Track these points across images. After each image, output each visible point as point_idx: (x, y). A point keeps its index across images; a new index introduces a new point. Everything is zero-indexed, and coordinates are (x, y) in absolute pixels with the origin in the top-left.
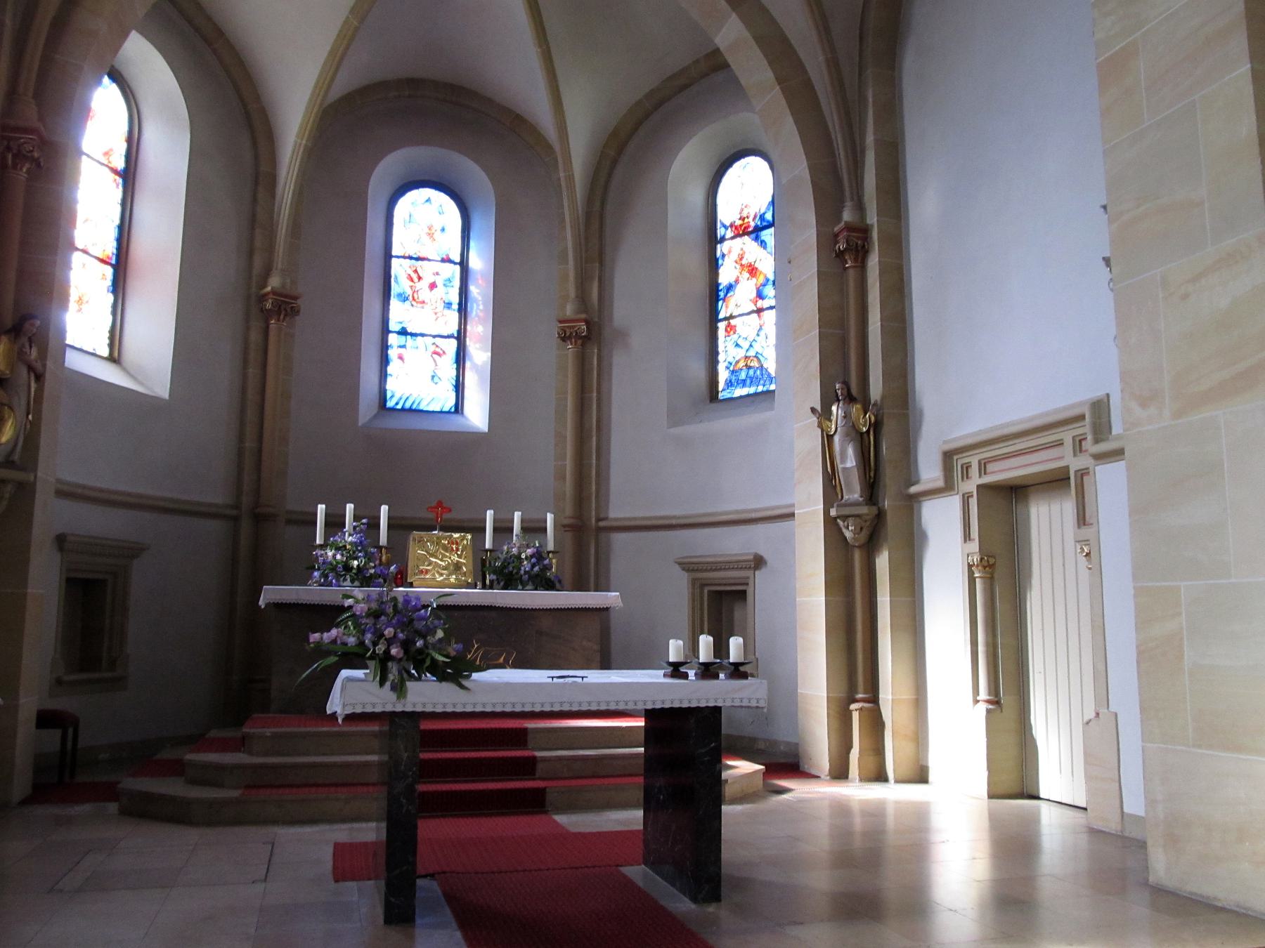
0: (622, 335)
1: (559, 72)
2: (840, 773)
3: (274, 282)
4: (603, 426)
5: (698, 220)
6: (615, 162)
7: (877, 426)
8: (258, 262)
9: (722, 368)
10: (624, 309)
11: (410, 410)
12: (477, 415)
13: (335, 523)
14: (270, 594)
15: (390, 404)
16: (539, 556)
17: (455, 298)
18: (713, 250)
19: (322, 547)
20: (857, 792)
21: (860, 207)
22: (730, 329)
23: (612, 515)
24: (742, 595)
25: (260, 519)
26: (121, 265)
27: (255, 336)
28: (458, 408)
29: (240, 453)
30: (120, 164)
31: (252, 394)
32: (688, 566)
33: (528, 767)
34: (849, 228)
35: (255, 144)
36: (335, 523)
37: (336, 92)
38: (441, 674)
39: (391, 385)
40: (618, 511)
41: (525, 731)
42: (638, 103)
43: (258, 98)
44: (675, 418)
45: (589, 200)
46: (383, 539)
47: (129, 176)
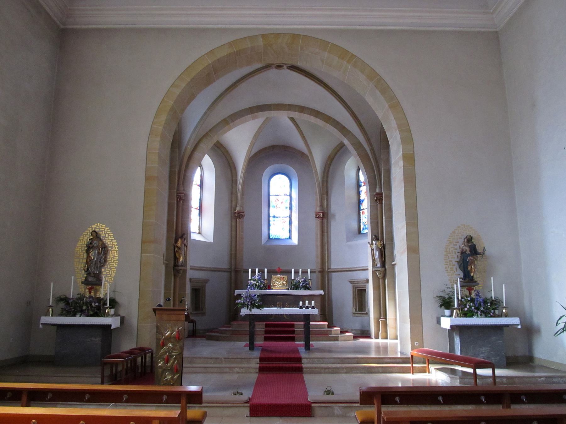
0: (334, 216)
1: (310, 145)
2: (377, 337)
3: (238, 209)
4: (328, 242)
5: (354, 181)
6: (330, 165)
7: (384, 246)
8: (234, 203)
9: (361, 224)
10: (334, 208)
11: (277, 239)
12: (295, 240)
13: (254, 272)
14: (237, 292)
15: (271, 237)
16: (305, 281)
17: (288, 206)
18: (358, 189)
19: (251, 280)
20: (380, 341)
21: (381, 188)
22: (363, 212)
23: (332, 267)
24: (365, 290)
25: (237, 272)
26: (200, 209)
27: (233, 224)
28: (290, 238)
29: (231, 254)
30: (199, 183)
31: (234, 239)
32: (351, 282)
33: (293, 332)
34: (377, 194)
35: (232, 172)
36: (254, 272)
37: (252, 153)
38: (258, 307)
39: (271, 232)
40: (333, 266)
41: (294, 324)
42: (336, 147)
43: (232, 160)
44: (348, 239)
45: (323, 177)
46: (266, 278)
47: (201, 186)
